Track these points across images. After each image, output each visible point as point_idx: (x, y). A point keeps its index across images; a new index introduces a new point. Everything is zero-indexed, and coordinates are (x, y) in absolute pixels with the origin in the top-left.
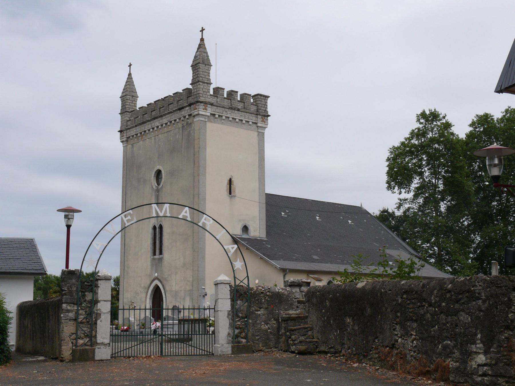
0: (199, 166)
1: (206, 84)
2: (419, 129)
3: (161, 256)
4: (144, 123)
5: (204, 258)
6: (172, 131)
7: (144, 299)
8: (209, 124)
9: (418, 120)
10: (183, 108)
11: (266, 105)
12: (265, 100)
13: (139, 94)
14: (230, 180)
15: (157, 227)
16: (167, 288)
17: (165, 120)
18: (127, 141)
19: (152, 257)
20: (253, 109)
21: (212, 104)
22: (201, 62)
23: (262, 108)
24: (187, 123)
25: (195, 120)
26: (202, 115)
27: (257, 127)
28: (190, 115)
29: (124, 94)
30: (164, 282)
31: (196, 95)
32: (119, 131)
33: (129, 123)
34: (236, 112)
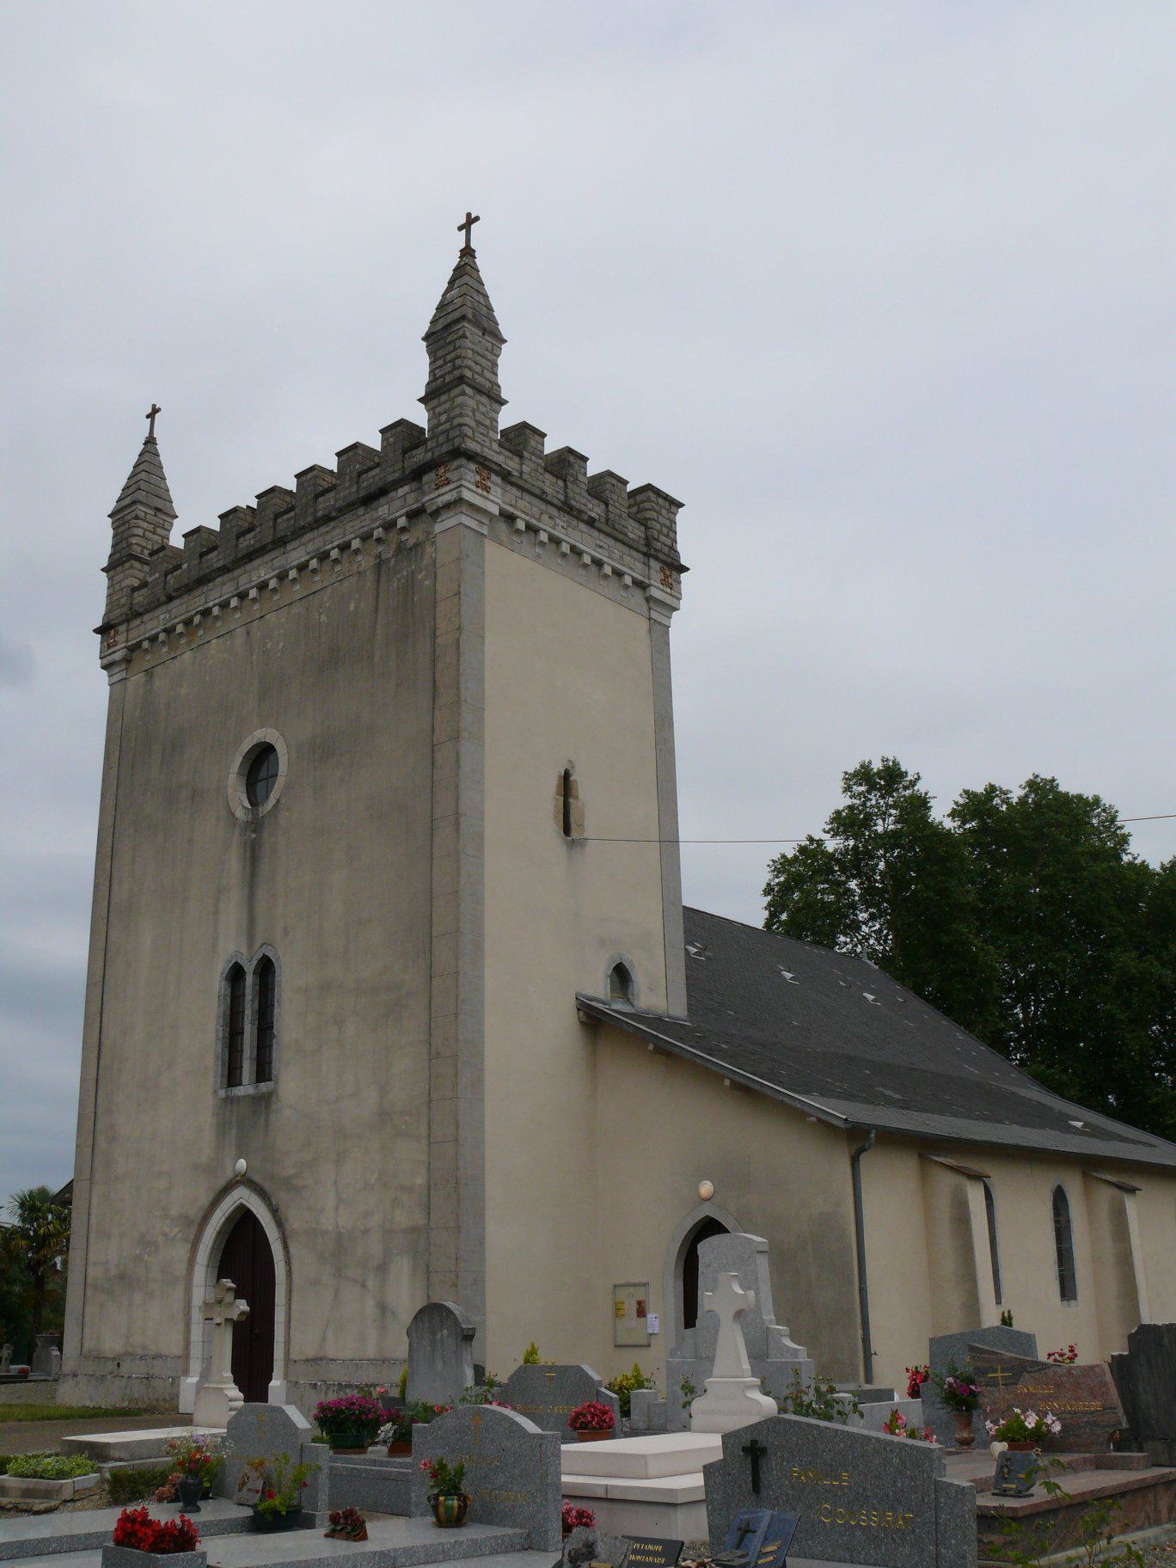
0: (458, 703)
1: (484, 400)
2: (851, 808)
3: (264, 1087)
4: (203, 581)
5: (478, 1084)
6: (329, 590)
7: (180, 1270)
8: (490, 548)
9: (848, 789)
10: (383, 491)
11: (671, 529)
12: (669, 511)
13: (177, 507)
14: (566, 776)
15: (249, 968)
16: (295, 1221)
17: (297, 554)
18: (127, 661)
19: (222, 1093)
20: (630, 534)
21: (506, 476)
22: (470, 316)
23: (662, 538)
24: (400, 548)
25: (438, 528)
26: (471, 505)
27: (649, 599)
28: (413, 515)
29: (127, 501)
30: (281, 1196)
31: (447, 431)
32: (97, 631)
33: (139, 597)
34: (582, 526)
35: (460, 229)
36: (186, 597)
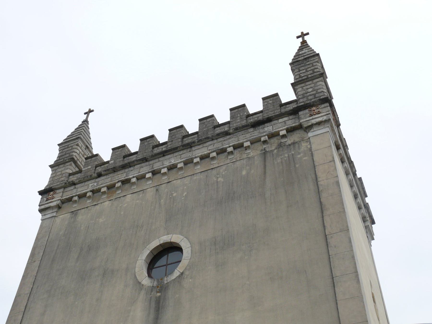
6: (224, 168)
25: (310, 134)
35: (85, 114)
36: (111, 175)
